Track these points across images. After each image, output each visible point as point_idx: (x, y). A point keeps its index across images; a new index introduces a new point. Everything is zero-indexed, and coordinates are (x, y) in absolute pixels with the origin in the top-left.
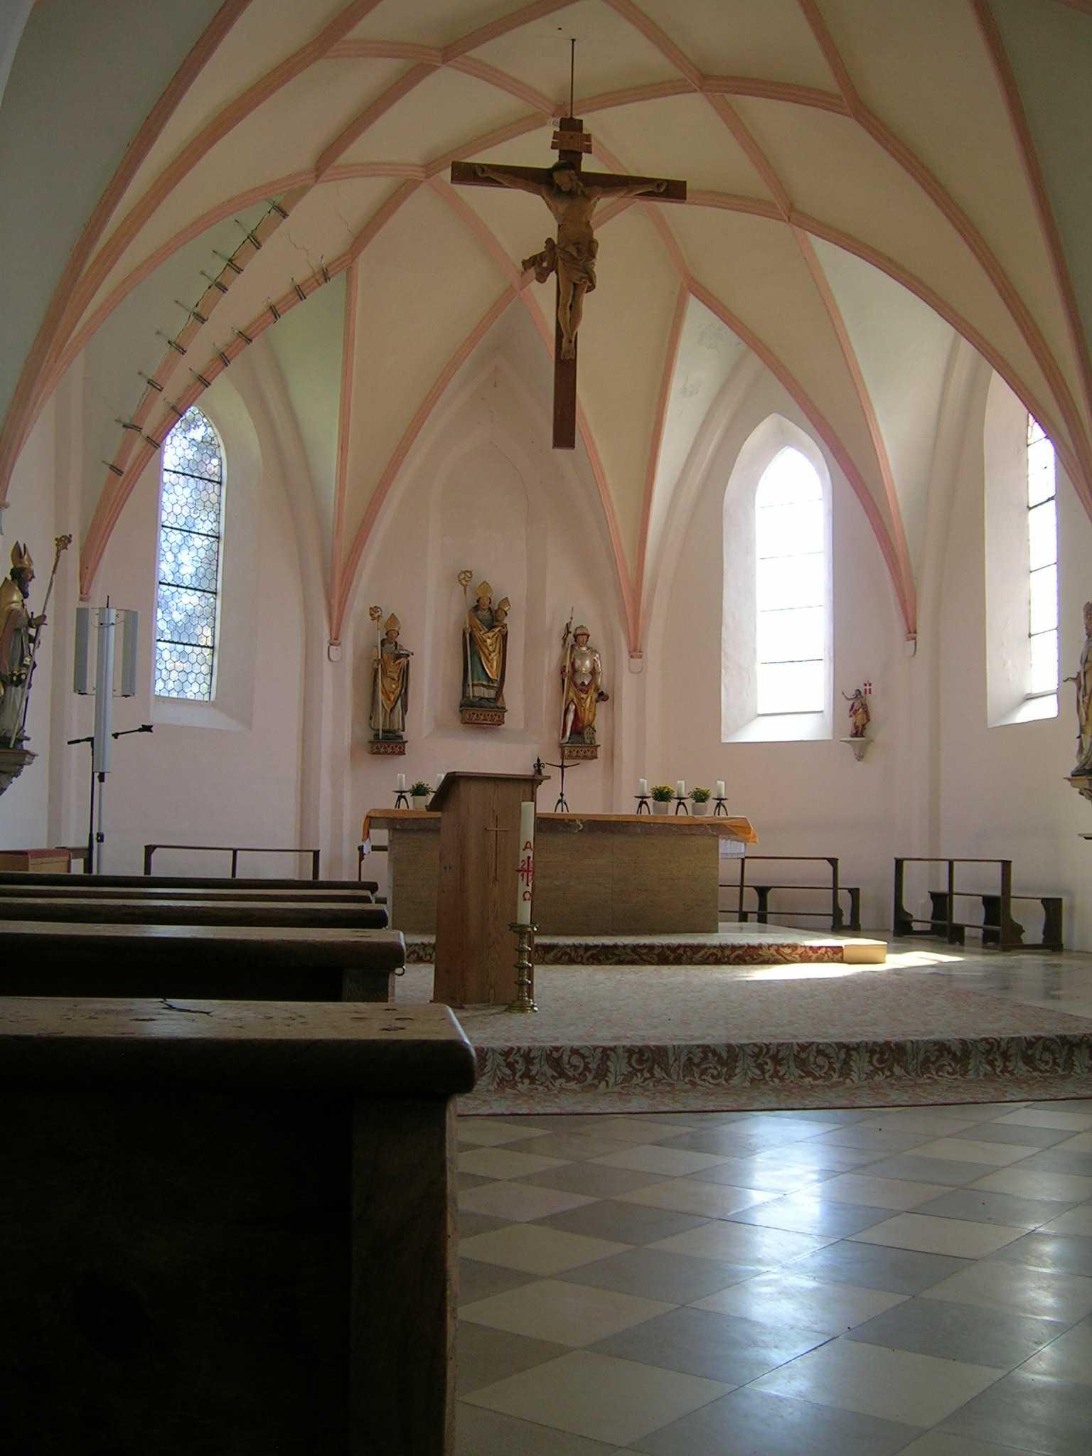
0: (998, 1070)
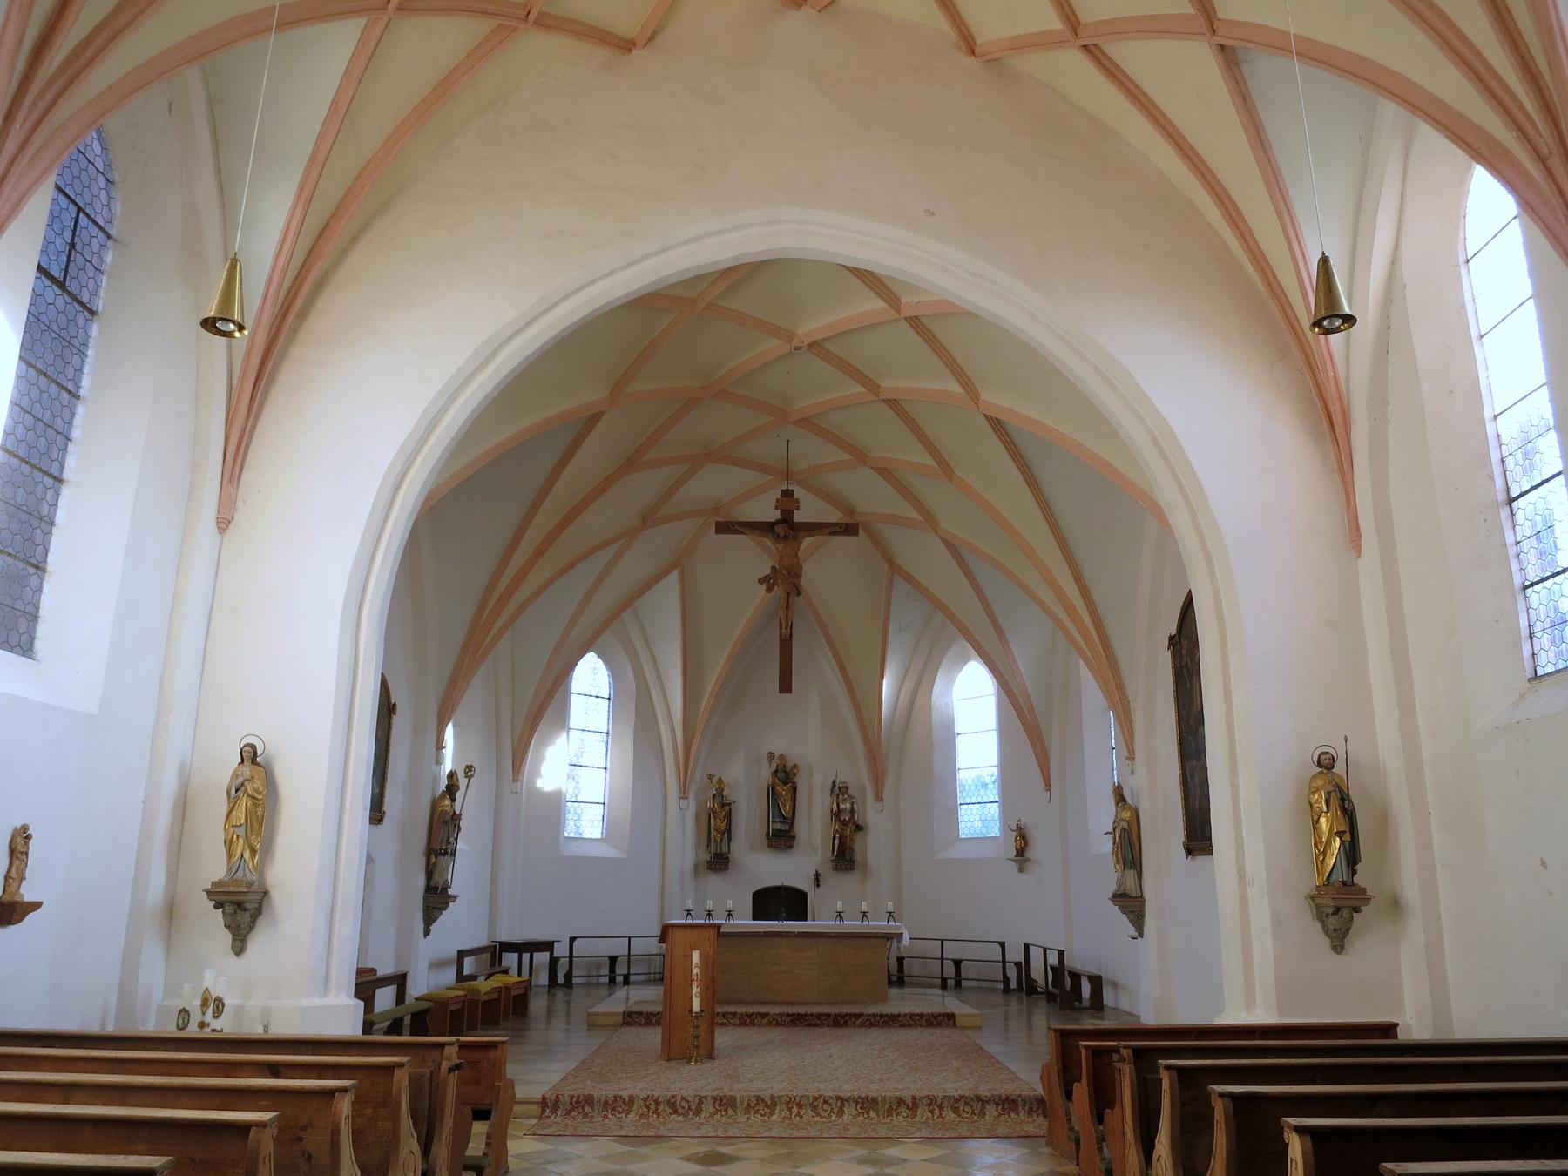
0: (935, 1116)
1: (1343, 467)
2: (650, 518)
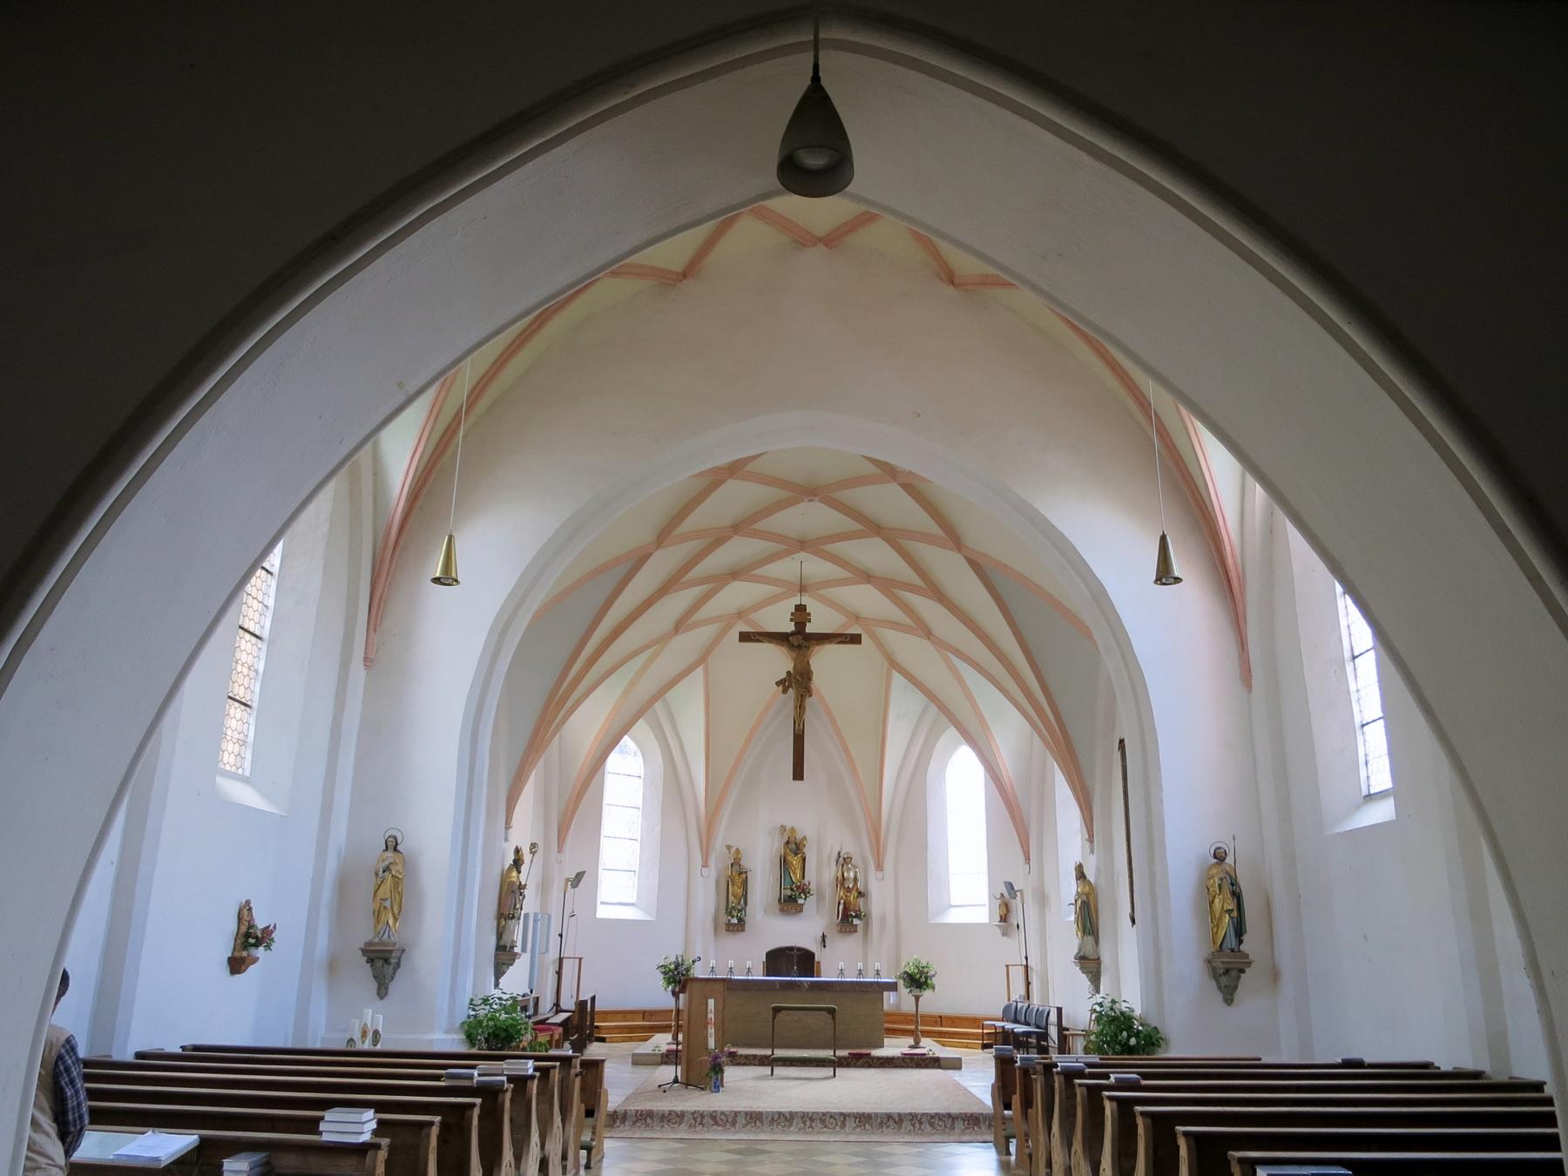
1: (1237, 620)
2: (680, 626)
